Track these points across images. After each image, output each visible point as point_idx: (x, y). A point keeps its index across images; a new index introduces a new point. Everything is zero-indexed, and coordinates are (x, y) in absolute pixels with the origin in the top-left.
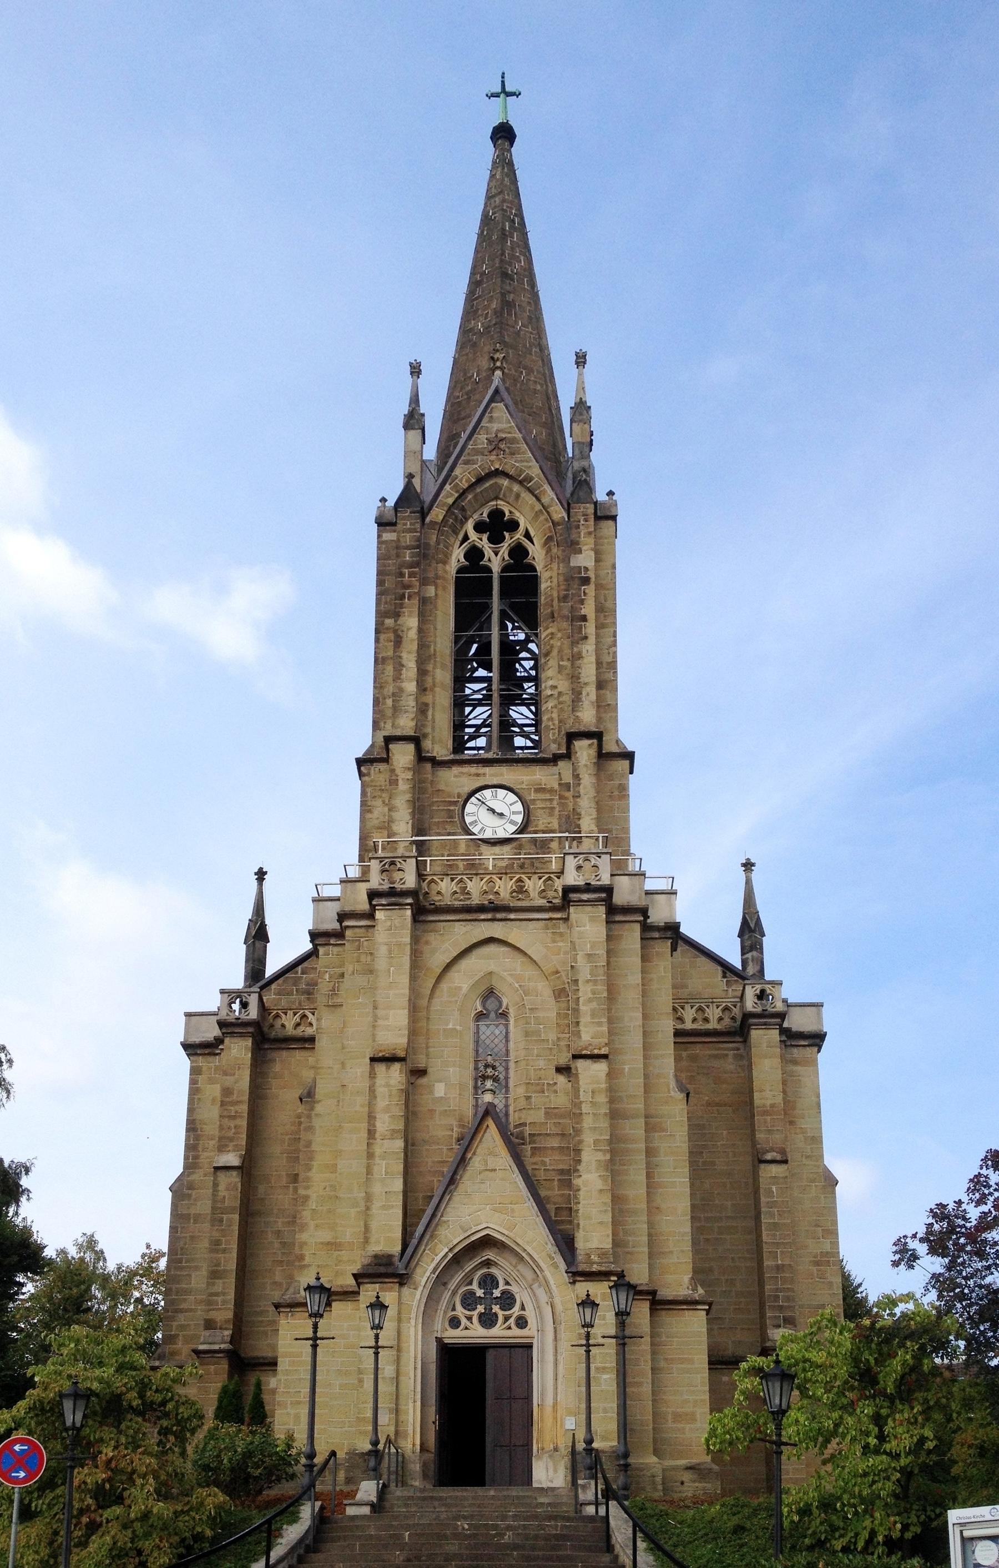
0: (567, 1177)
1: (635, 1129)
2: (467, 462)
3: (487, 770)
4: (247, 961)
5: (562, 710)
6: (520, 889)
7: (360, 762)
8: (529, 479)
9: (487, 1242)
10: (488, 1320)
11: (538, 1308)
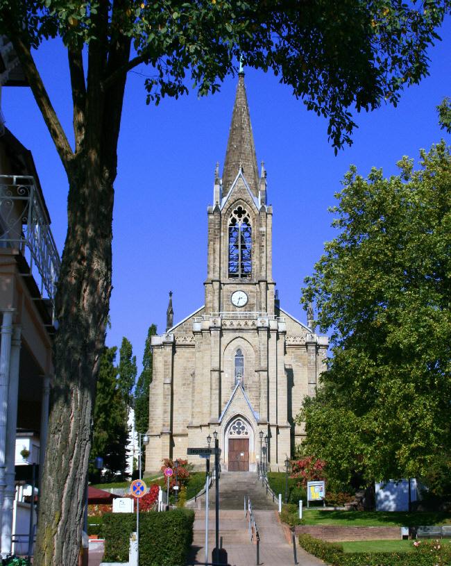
8: (249, 201)
9: (239, 415)
10: (239, 433)
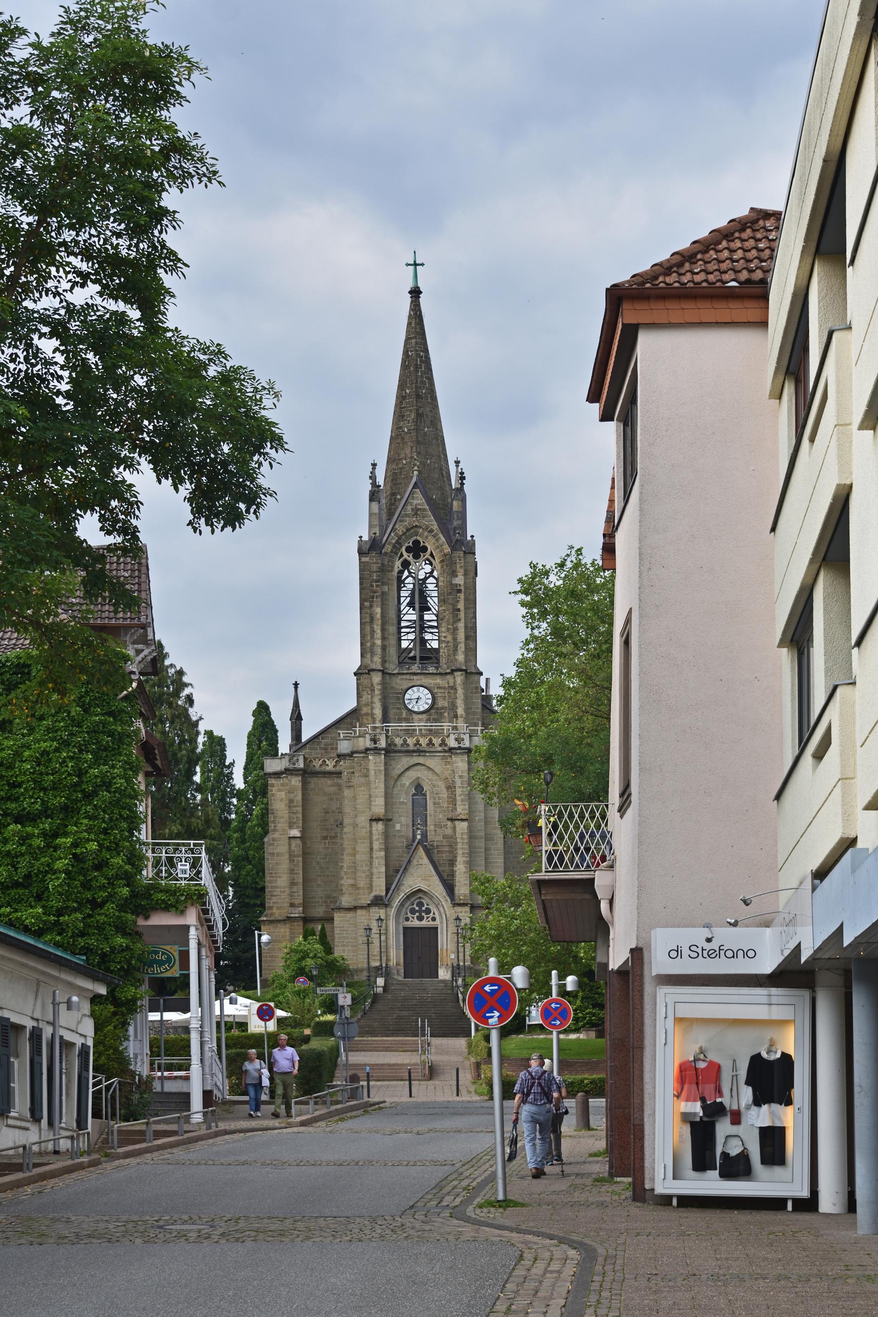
0: (452, 862)
1: (481, 844)
2: (402, 521)
3: (415, 677)
4: (292, 730)
5: (448, 650)
6: (430, 743)
7: (355, 674)
9: (420, 891)
10: (420, 918)
11: (440, 914)
